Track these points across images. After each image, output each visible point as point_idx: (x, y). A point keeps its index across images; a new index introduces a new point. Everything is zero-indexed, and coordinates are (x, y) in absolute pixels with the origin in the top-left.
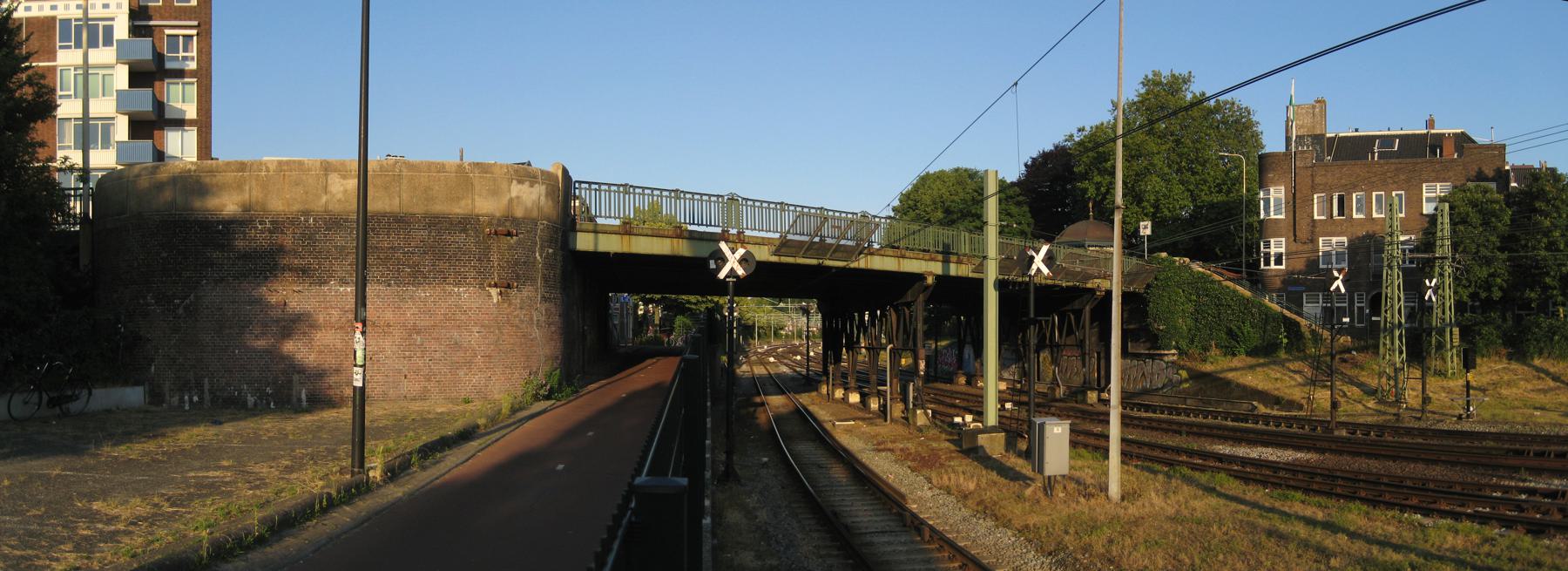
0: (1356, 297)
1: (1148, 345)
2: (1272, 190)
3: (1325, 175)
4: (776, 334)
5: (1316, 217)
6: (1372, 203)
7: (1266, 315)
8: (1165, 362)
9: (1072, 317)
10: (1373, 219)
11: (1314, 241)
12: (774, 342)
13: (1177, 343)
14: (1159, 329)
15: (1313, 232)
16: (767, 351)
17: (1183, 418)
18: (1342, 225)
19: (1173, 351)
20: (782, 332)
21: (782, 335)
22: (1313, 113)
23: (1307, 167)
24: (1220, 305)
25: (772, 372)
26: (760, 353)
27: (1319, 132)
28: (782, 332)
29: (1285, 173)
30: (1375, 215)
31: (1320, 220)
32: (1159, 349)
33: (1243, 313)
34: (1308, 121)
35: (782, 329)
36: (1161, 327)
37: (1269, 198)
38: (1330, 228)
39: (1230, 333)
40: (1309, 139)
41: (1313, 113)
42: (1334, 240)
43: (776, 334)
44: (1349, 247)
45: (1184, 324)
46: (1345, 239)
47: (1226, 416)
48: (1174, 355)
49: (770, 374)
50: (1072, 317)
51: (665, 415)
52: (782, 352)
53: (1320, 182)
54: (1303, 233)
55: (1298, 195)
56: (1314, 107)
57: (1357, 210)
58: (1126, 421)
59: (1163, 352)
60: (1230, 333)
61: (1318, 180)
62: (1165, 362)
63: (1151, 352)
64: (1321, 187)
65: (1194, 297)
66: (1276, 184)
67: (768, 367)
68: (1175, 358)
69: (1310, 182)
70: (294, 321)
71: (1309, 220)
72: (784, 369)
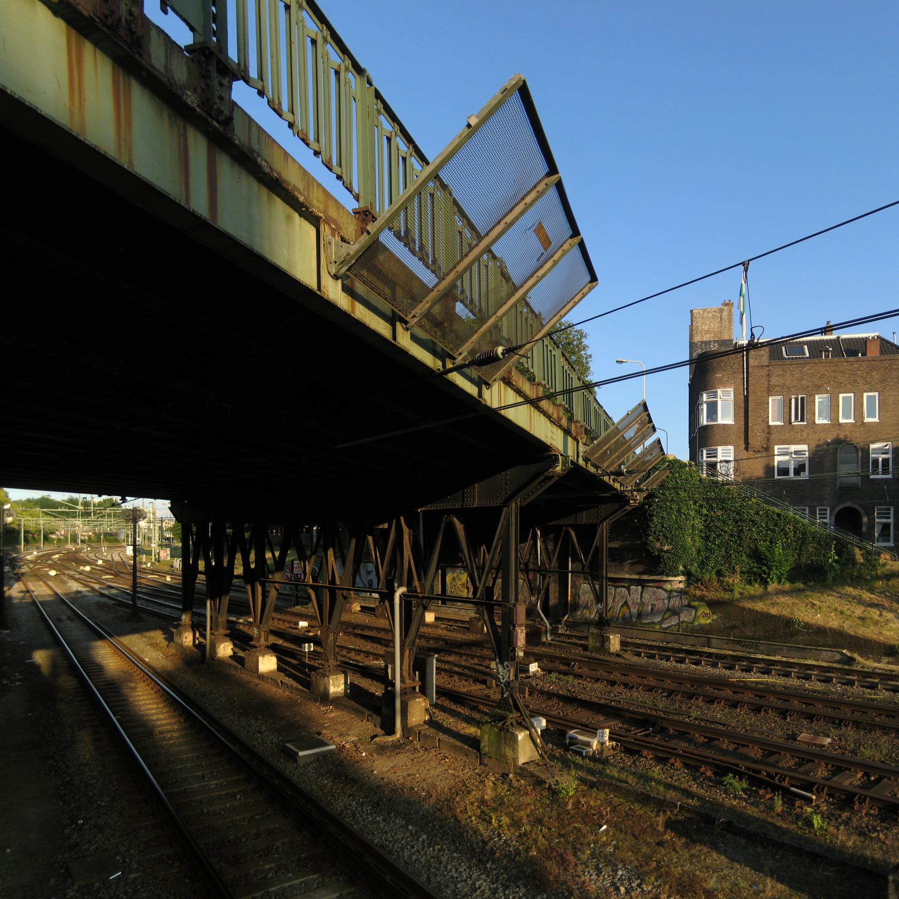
0: (818, 512)
1: (641, 568)
2: (719, 392)
3: (782, 375)
4: (46, 538)
5: (771, 423)
6: (838, 413)
7: (804, 534)
8: (666, 590)
9: (459, 527)
10: (840, 425)
11: (768, 450)
12: (46, 549)
13: (685, 567)
14: (661, 550)
15: (768, 439)
16: (38, 557)
17: (669, 665)
18: (802, 431)
19: (680, 578)
20: (53, 536)
21: (53, 540)
22: (721, 317)
23: (762, 366)
24: (740, 520)
25: (59, 591)
26: (31, 562)
27: (727, 338)
28: (53, 536)
29: (734, 373)
30: (842, 421)
31: (777, 426)
32: (661, 573)
33: (774, 531)
34: (715, 325)
35: (53, 533)
36: (666, 548)
37: (716, 402)
38: (788, 434)
39: (757, 556)
40: (716, 345)
41: (721, 317)
42: (793, 448)
43: (46, 538)
44: (810, 459)
45: (692, 541)
46: (804, 447)
47: (785, 670)
48: (680, 582)
49: (56, 594)
50: (459, 527)
51: (200, 718)
52: (60, 559)
53: (776, 384)
54: (757, 439)
55: (751, 398)
56: (721, 311)
57: (819, 416)
58: (205, 616)
59: (665, 578)
60: (757, 556)
61: (774, 381)
62: (666, 590)
63: (645, 577)
64: (778, 389)
65: (705, 511)
66: (724, 384)
67: (50, 583)
68: (682, 586)
69: (766, 383)
70: (358, 213)
71: (764, 426)
72: (75, 586)
